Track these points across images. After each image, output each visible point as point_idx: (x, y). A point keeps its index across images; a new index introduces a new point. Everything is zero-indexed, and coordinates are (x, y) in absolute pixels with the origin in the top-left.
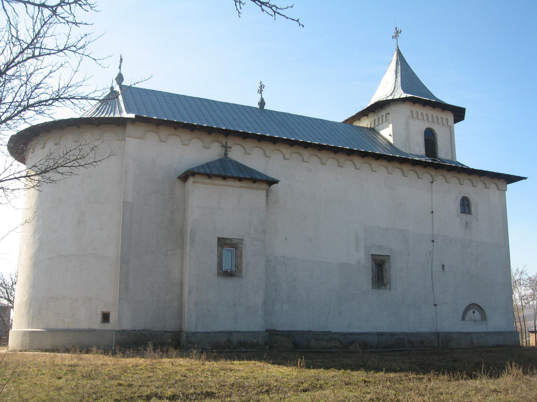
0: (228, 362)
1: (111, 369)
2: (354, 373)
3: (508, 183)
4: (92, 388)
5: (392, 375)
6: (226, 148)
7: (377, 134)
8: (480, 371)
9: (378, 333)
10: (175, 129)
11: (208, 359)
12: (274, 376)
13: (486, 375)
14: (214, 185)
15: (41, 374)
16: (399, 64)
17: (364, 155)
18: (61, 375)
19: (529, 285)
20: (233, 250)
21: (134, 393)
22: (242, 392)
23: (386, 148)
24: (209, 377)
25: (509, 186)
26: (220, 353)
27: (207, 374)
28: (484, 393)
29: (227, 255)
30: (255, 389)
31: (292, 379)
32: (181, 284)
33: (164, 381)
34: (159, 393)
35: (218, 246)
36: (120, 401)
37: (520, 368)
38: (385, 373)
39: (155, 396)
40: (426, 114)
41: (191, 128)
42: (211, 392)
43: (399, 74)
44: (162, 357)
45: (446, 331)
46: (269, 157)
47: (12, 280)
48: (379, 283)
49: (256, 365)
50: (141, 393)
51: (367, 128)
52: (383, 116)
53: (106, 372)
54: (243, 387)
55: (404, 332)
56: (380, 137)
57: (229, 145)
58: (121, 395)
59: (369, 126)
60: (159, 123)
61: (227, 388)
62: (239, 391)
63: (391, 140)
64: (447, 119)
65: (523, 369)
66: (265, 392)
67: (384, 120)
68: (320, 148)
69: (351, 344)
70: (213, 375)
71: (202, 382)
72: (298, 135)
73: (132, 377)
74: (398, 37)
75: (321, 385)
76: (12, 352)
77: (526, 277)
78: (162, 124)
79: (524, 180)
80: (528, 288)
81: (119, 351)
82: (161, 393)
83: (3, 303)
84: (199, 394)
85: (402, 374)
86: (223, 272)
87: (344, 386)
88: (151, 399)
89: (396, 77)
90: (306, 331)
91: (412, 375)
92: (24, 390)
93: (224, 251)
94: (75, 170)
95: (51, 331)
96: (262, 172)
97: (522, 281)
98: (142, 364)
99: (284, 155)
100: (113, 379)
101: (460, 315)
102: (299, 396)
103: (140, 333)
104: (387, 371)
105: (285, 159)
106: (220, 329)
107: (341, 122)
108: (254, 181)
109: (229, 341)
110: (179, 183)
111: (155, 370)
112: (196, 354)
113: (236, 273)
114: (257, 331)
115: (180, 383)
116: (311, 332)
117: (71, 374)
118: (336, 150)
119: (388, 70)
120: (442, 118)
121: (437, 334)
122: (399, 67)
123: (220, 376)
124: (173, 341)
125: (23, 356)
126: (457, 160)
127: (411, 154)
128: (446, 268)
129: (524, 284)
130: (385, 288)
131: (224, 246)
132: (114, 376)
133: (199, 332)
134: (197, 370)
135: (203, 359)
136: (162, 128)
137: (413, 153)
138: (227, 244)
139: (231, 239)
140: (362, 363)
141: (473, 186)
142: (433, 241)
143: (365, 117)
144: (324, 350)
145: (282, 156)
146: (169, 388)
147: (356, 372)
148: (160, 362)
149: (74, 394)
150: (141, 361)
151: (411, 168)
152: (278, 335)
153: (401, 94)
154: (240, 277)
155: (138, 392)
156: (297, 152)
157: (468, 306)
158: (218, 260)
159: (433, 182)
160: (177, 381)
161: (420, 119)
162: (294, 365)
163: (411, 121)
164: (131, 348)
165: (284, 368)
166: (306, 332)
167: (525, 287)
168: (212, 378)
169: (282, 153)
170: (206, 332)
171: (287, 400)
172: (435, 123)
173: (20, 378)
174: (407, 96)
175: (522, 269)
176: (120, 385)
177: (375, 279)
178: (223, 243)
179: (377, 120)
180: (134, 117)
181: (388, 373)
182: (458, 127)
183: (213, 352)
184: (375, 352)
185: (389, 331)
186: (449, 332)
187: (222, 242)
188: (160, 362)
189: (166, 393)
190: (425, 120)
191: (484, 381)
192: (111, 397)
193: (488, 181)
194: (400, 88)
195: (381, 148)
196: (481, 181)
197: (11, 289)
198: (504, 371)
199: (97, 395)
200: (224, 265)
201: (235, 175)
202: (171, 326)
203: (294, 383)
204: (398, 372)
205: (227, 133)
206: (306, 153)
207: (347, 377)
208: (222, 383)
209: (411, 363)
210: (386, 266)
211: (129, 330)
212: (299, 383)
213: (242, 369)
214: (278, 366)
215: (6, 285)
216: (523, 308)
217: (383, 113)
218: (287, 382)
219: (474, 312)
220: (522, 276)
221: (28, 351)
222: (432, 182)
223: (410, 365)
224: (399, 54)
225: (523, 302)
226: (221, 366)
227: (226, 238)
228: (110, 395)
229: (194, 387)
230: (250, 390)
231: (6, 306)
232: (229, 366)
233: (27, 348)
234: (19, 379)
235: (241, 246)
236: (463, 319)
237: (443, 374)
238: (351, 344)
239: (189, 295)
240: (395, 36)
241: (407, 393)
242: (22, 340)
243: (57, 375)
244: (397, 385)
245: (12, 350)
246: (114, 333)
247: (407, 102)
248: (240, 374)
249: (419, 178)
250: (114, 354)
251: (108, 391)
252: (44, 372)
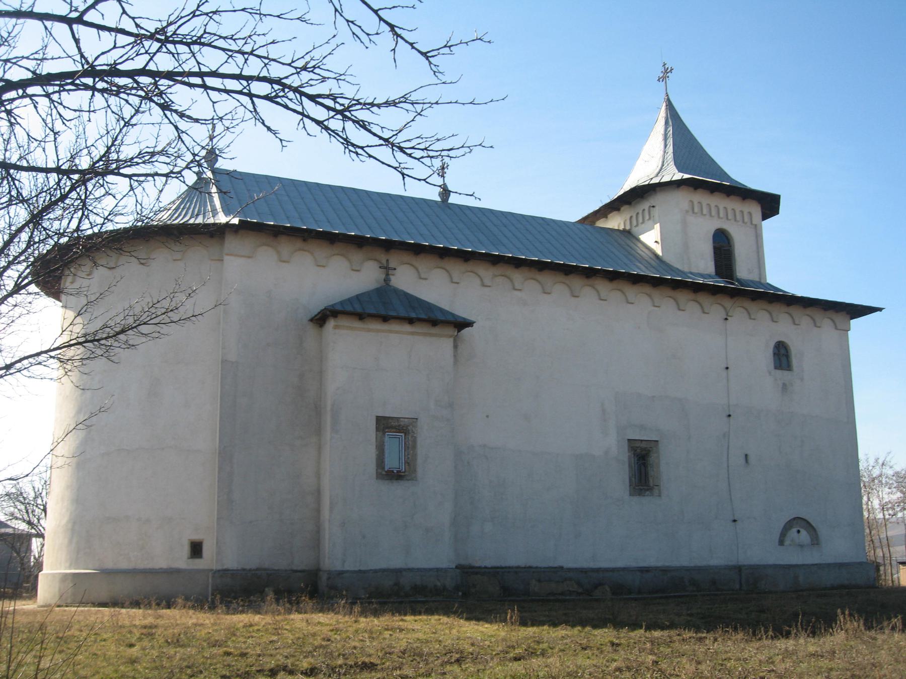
0: (397, 618)
1: (210, 631)
2: (596, 632)
3: (852, 318)
4: (184, 660)
5: (657, 634)
6: (387, 270)
7: (634, 241)
8: (796, 626)
9: (641, 567)
10: (305, 240)
11: (364, 613)
12: (470, 637)
13: (806, 632)
14: (369, 330)
15: (101, 640)
16: (671, 123)
17: (613, 276)
18: (133, 641)
19: (895, 485)
21: (251, 666)
22: (419, 663)
23: (649, 264)
24: (366, 641)
25: (853, 322)
26: (383, 604)
27: (362, 636)
28: (797, 659)
29: (393, 445)
30: (438, 657)
31: (497, 642)
32: (318, 493)
33: (296, 649)
34: (289, 665)
35: (377, 429)
36: (229, 677)
37: (859, 619)
38: (646, 631)
39: (284, 670)
40: (716, 206)
41: (329, 238)
42: (371, 663)
43: (670, 141)
44: (289, 612)
45: (752, 563)
46: (458, 283)
47: (34, 489)
48: (642, 486)
49: (441, 621)
50: (261, 665)
51: (618, 230)
52: (644, 210)
53: (203, 635)
54: (421, 655)
55: (684, 567)
56: (640, 245)
57: (392, 265)
58: (231, 669)
59: (622, 228)
60: (277, 232)
61: (394, 657)
62: (415, 662)
63: (659, 251)
64: (750, 214)
65: (866, 621)
66: (455, 661)
67: (647, 217)
68: (541, 266)
69: (596, 586)
70: (373, 638)
71: (355, 648)
72: (504, 245)
73: (245, 642)
74: (667, 79)
75: (543, 650)
76: (45, 609)
77: (890, 472)
78: (283, 233)
79: (878, 312)
80: (895, 490)
81: (221, 603)
82: (292, 665)
83: (20, 528)
84: (351, 666)
85: (673, 633)
86: (386, 472)
87: (580, 651)
88: (277, 675)
89: (666, 146)
90: (523, 566)
91: (687, 634)
92: (79, 664)
93: (387, 439)
94: (165, 329)
95: (108, 573)
96: (447, 308)
97: (884, 479)
98: (259, 622)
99: (482, 280)
100: (214, 646)
101: (776, 536)
102: (507, 666)
104: (649, 628)
105: (483, 285)
106: (383, 565)
107: (576, 222)
108: (434, 323)
110: (312, 330)
111: (280, 632)
112: (344, 607)
113: (406, 473)
114: (442, 569)
115: (321, 650)
116: (530, 567)
117: (148, 639)
118: (567, 270)
119: (652, 133)
120: (742, 212)
121: (739, 569)
122: (671, 129)
123: (384, 639)
124: (307, 586)
125: (64, 613)
126: (768, 281)
127: (691, 273)
128: (752, 459)
129: (887, 483)
130: (652, 495)
131: (386, 430)
132: (217, 641)
133: (347, 571)
134: (347, 631)
135: (356, 614)
136: (283, 239)
137: (694, 270)
138: (392, 427)
139: (398, 419)
140: (611, 617)
141: (795, 324)
142: (729, 416)
143: (615, 213)
144: (552, 598)
145: (478, 281)
146: (305, 657)
147: (601, 630)
148: (286, 619)
149: (156, 668)
150: (257, 618)
151: (691, 296)
152: (477, 573)
153: (673, 174)
154: (413, 480)
155: (257, 665)
156: (503, 274)
157: (790, 521)
158: (377, 453)
159: (728, 318)
160: (316, 647)
161: (705, 215)
162: (501, 621)
163: (691, 219)
164: (240, 597)
165: (486, 626)
166: (522, 568)
167: (889, 488)
168: (371, 642)
169: (479, 276)
170: (360, 571)
171: (488, 672)
172: (730, 220)
173: (69, 646)
174: (684, 178)
175: (884, 459)
176: (228, 654)
177: (633, 479)
178: (384, 424)
179: (634, 218)
180: (237, 223)
181: (650, 631)
182: (769, 226)
183: (372, 603)
184: (636, 599)
185: (660, 564)
186: (758, 565)
187: (384, 424)
188: (286, 619)
189: (300, 666)
190: (713, 216)
191: (802, 641)
192: (215, 672)
193: (818, 314)
194: (673, 163)
195: (642, 264)
196: (808, 315)
197: (33, 505)
198: (834, 625)
199: (193, 670)
200: (386, 461)
201: (403, 314)
202: (301, 561)
203: (500, 648)
204: (666, 630)
205: (389, 246)
206: (518, 276)
207: (585, 638)
208: (388, 650)
209: (691, 615)
210: (652, 459)
211: (235, 568)
212: (509, 647)
213: (419, 628)
214: (476, 623)
215: (25, 499)
216: (887, 523)
217: (645, 205)
218: (489, 646)
219: (799, 532)
220: (883, 470)
221: (71, 606)
222: (726, 319)
223: (689, 618)
224: (670, 106)
225: (886, 512)
226: (386, 624)
227: (389, 418)
228: (214, 669)
229: (344, 655)
230: (431, 659)
231: (25, 533)
232: (397, 623)
233: (69, 601)
234: (69, 649)
235: (413, 429)
236: (781, 542)
237: (735, 629)
238: (596, 586)
239: (331, 509)
240: (662, 77)
241: (676, 660)
242: (60, 589)
243: (127, 642)
244: (661, 649)
245: (44, 604)
246: (210, 574)
247: (683, 186)
248: (416, 635)
249: (704, 312)
250: (213, 608)
251: (210, 664)
252: (105, 636)
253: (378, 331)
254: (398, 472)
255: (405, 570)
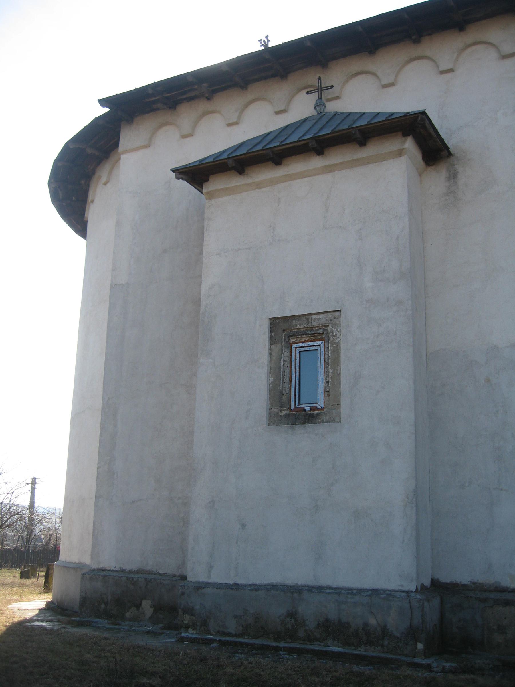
14: (259, 186)
20: (296, 348)
35: (272, 340)
103: (128, 578)
109: (292, 614)
139: (307, 316)
145: (493, 54)
154: (334, 421)
235: (335, 330)
253: (273, 182)
254: (311, 409)
255: (310, 589)
